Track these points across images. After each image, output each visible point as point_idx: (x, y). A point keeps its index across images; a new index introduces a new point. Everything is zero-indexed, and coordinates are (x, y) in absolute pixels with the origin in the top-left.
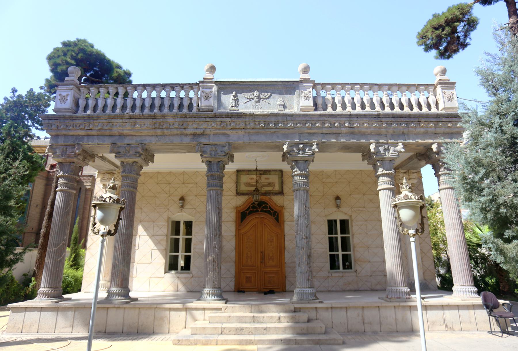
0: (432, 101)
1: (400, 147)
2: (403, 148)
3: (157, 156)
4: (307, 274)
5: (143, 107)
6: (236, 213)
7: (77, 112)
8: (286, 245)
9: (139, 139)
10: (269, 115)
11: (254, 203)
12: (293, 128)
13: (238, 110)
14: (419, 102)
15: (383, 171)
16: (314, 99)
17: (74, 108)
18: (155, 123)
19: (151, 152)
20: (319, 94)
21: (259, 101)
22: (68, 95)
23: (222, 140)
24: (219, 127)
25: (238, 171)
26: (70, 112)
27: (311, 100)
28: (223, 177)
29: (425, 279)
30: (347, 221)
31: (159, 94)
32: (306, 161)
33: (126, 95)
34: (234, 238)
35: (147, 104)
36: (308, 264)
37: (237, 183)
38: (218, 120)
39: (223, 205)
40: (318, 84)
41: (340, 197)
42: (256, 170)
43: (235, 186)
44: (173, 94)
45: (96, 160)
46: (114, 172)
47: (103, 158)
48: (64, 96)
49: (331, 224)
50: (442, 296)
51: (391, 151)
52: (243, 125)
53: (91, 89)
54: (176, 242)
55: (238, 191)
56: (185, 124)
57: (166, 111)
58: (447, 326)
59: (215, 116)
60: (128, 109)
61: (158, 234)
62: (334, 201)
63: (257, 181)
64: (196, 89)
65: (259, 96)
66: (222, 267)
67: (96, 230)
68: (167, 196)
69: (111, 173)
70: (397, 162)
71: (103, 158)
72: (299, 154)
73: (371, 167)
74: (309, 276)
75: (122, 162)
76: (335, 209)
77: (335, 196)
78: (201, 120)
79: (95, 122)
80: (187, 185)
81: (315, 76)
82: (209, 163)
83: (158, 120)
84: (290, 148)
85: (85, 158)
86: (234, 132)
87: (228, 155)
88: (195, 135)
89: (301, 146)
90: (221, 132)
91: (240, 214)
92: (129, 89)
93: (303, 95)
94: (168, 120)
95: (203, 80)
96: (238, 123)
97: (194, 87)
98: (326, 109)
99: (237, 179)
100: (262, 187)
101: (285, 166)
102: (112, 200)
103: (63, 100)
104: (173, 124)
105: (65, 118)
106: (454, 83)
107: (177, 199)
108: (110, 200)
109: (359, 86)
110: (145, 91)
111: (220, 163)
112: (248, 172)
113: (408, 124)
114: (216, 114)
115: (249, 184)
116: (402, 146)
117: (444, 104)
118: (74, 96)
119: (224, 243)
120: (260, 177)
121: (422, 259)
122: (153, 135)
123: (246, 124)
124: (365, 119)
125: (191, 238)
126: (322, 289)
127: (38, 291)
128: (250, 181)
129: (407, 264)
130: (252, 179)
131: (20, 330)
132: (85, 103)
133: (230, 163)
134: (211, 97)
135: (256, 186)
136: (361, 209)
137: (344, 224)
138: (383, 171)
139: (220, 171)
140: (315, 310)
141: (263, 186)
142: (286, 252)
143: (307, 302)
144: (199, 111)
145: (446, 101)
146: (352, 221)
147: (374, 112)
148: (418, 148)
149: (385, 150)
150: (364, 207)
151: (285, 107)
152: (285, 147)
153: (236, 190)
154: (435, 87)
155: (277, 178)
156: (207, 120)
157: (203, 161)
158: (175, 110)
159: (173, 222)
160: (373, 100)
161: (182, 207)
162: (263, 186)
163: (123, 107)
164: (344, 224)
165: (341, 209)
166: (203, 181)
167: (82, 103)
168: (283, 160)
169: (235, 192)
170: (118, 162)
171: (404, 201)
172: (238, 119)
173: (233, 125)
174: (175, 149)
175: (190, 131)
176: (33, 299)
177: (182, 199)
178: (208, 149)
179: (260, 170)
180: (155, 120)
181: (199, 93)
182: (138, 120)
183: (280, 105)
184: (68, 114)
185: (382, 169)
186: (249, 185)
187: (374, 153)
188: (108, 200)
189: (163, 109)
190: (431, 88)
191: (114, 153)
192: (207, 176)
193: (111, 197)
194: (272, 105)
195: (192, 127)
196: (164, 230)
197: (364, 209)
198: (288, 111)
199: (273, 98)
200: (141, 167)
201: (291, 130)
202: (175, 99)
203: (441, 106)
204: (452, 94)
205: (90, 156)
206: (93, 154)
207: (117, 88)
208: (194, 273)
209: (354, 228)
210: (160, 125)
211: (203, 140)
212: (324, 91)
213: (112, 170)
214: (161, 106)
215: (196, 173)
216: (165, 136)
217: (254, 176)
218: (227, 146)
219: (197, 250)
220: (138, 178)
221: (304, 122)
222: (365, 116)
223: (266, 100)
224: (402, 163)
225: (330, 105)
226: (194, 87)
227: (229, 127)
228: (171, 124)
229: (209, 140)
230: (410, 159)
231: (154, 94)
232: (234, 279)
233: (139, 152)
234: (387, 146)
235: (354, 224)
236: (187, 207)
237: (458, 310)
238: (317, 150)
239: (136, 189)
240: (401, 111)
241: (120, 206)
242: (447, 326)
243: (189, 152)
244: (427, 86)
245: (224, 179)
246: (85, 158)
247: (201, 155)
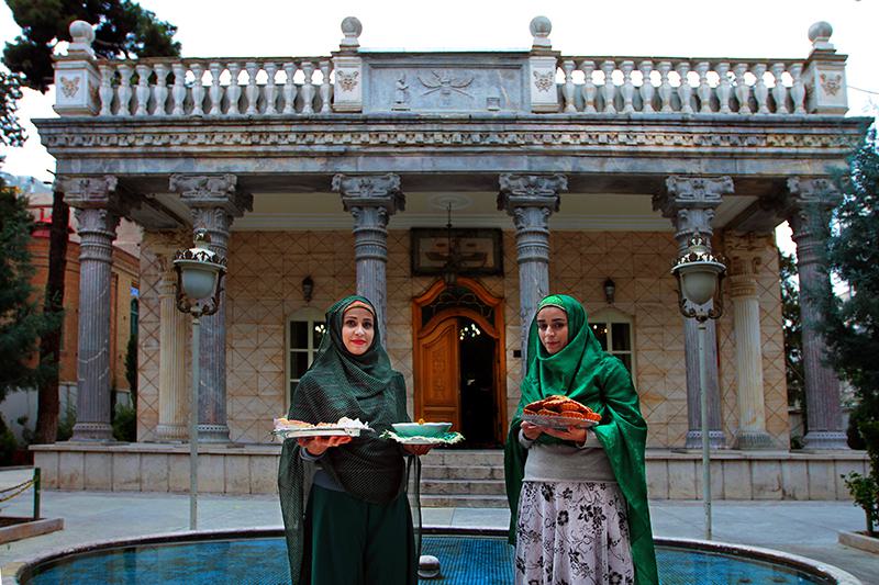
22: (77, 80)
30: (628, 325)
33: (170, 79)
40: (569, 58)
43: (408, 260)
44: (281, 77)
48: (70, 82)
58: (784, 492)
61: (266, 344)
63: (451, 250)
67: (183, 306)
76: (603, 305)
77: (602, 280)
81: (561, 42)
91: (420, 311)
92: (177, 69)
95: (338, 49)
103: (69, 89)
105: (79, 124)
106: (843, 58)
107: (298, 282)
108: (203, 257)
110: (226, 72)
112: (434, 232)
120: (457, 244)
124: (657, 129)
128: (437, 249)
130: (443, 245)
131: (55, 486)
134: (355, 84)
136: (654, 304)
150: (660, 302)
162: (465, 259)
163: (185, 103)
169: (408, 270)
177: (308, 281)
179: (457, 230)
186: (435, 256)
188: (199, 256)
189: (263, 107)
193: (204, 253)
197: (660, 305)
202: (285, 87)
213: (171, 226)
217: (445, 241)
222: (658, 122)
224: (737, 217)
225: (630, 100)
226: (321, 63)
231: (244, 78)
240: (771, 115)
242: (784, 492)
243: (319, 190)
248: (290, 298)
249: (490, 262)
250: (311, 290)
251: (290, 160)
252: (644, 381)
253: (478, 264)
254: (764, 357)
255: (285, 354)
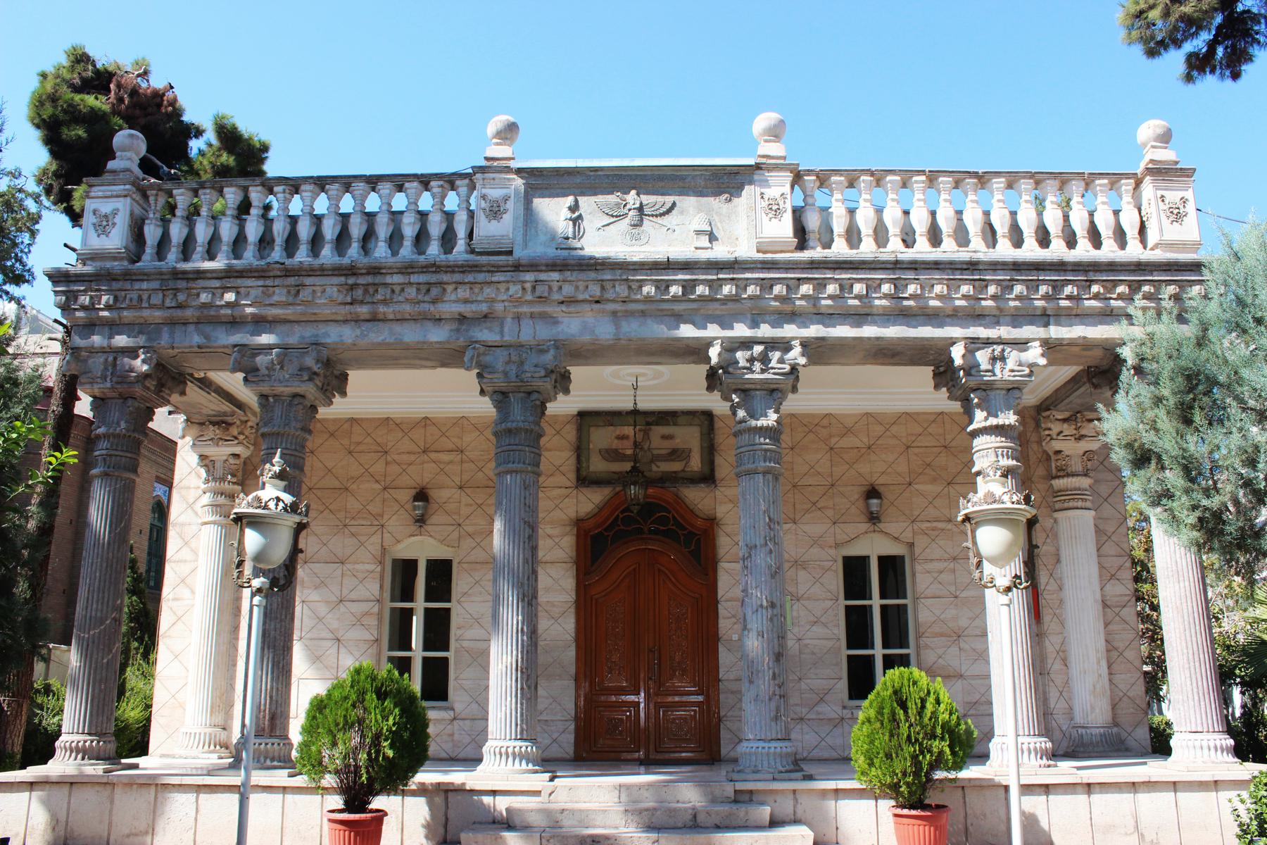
0: (1129, 222)
1: (1035, 354)
2: (1043, 355)
3: (355, 376)
4: (773, 705)
5: (316, 241)
6: (578, 536)
7: (139, 259)
8: (722, 631)
9: (308, 332)
10: (669, 265)
11: (627, 510)
12: (734, 299)
13: (582, 249)
14: (1092, 223)
15: (986, 419)
16: (798, 214)
17: (132, 247)
18: (352, 287)
19: (339, 367)
20: (810, 200)
21: (639, 224)
23: (528, 333)
24: (529, 297)
25: (582, 415)
26: (122, 259)
27: (788, 218)
28: (540, 436)
29: (1116, 724)
31: (361, 201)
32: (773, 391)
34: (573, 610)
35: (330, 230)
36: (774, 677)
37: (580, 450)
38: (530, 277)
39: (541, 515)
40: (809, 172)
41: (881, 489)
42: (635, 412)
43: (573, 460)
45: (188, 390)
46: (229, 419)
47: (205, 384)
48: (106, 216)
49: (854, 570)
50: (1145, 763)
51: (1011, 364)
52: (595, 290)
53: (175, 192)
54: (402, 622)
55: (584, 473)
56: (435, 291)
57: (381, 251)
59: (518, 267)
60: (277, 248)
61: (353, 596)
62: (861, 504)
64: (463, 190)
65: (641, 209)
66: (541, 692)
68: (377, 486)
69: (221, 423)
70: (1030, 398)
71: (205, 384)
72: (750, 370)
73: (956, 406)
74: (778, 710)
75: (263, 397)
76: (865, 526)
77: (864, 489)
78: (481, 277)
79: (191, 284)
80: (433, 455)
82: (501, 398)
83: (362, 280)
84: (726, 355)
85: (161, 386)
86: (572, 309)
87: (554, 377)
88: (462, 319)
89: (758, 349)
90: (537, 309)
93: (765, 204)
94: (389, 279)
95: (484, 163)
96: (581, 285)
97: (458, 183)
98: (828, 245)
99: (579, 438)
100: (652, 461)
101: (715, 403)
102: (281, 504)
104: (403, 290)
107: (406, 496)
109: (923, 178)
111: (535, 396)
112: (611, 417)
113: (1057, 286)
114: (523, 262)
115: (616, 451)
116: (1039, 350)
117: (1161, 230)
118: (132, 214)
119: (543, 624)
120: (646, 434)
121: (1109, 668)
122: (346, 321)
123: (603, 288)
125: (448, 610)
126: (826, 755)
127: (57, 744)
128: (616, 444)
129: (1067, 682)
130: (622, 438)
132: (159, 232)
133: (560, 397)
134: (506, 211)
135: (635, 458)
136: (940, 525)
137: (892, 568)
138: (986, 419)
139: (531, 419)
140: (791, 796)
141: (656, 459)
142: (721, 648)
143: (770, 776)
144: (472, 251)
145: (1166, 222)
146: (913, 560)
147: (963, 255)
148: (1089, 353)
149: (994, 359)
150: (950, 521)
151: (712, 237)
152: (714, 353)
153: (578, 470)
154: (1138, 183)
155: (697, 435)
156: (498, 277)
157: (482, 392)
158: (407, 251)
159: (395, 561)
160: (965, 217)
161: (421, 521)
162: (656, 459)
164: (892, 568)
165: (881, 526)
166: (482, 447)
167: (152, 233)
168: (710, 388)
169: (573, 476)
170: (247, 395)
171: (986, 507)
172: (583, 276)
173: (568, 290)
174: (406, 358)
175: (450, 308)
176: (46, 763)
177: (422, 496)
178: (499, 359)
180: (351, 281)
181: (472, 200)
182: (308, 281)
183: (698, 233)
184: (117, 266)
185: (985, 414)
186: (612, 455)
187: (961, 368)
188: (272, 505)
189: (371, 245)
190: (1127, 186)
191: (240, 371)
192: (496, 434)
193: (278, 499)
194: (677, 233)
195: (453, 297)
196: (369, 589)
198: (720, 252)
199: (682, 213)
200: (314, 409)
201: (730, 305)
203: (1153, 236)
204: (1184, 201)
205: (174, 378)
206: (181, 374)
207: (245, 190)
208: (458, 707)
209: (923, 581)
210: (366, 292)
211: (486, 335)
212: (826, 190)
213: (225, 414)
214: (369, 236)
215: (460, 423)
216: (380, 324)
217: (629, 430)
218: (552, 352)
219: (465, 644)
220: (305, 440)
221: (767, 283)
223: (659, 220)
227: (556, 297)
228: (397, 289)
229: (502, 333)
230: (1074, 381)
232: (573, 727)
233: (309, 369)
234: (998, 348)
235: (918, 568)
236: (434, 519)
237: (1175, 791)
238: (802, 361)
239: (302, 470)
241: (297, 519)
243: (444, 365)
244: (1115, 179)
245: (543, 441)
246: (161, 386)
247: (480, 375)
248: (391, 522)
249: (696, 463)
250: (425, 508)
251: (406, 325)
252: (927, 647)
253: (676, 466)
254: (1105, 605)
255: (380, 614)
